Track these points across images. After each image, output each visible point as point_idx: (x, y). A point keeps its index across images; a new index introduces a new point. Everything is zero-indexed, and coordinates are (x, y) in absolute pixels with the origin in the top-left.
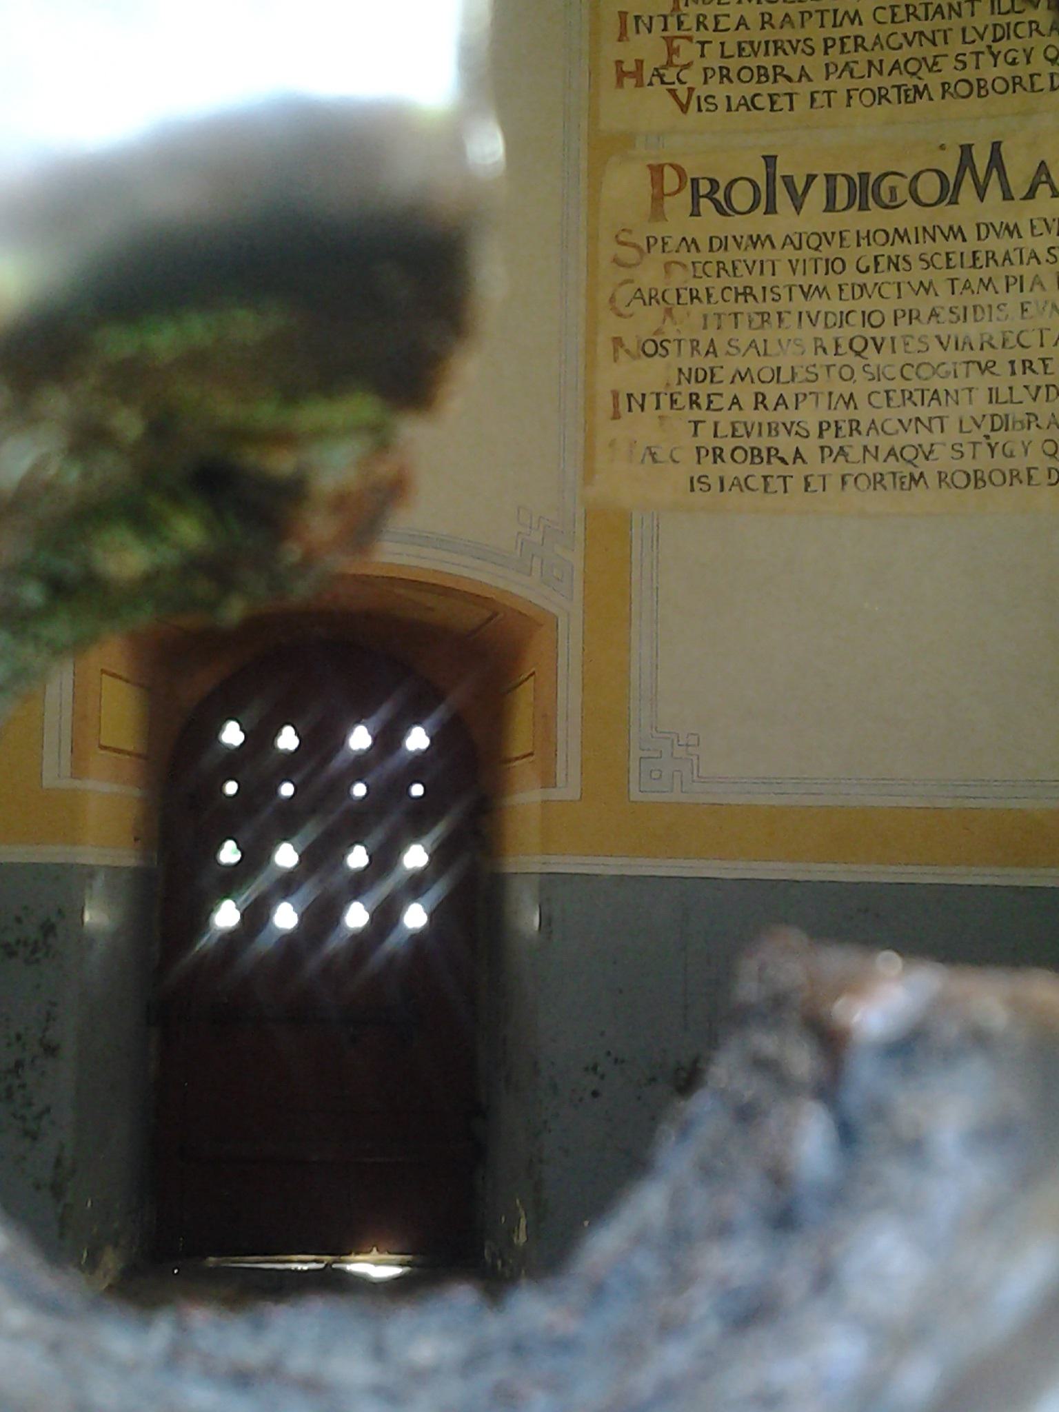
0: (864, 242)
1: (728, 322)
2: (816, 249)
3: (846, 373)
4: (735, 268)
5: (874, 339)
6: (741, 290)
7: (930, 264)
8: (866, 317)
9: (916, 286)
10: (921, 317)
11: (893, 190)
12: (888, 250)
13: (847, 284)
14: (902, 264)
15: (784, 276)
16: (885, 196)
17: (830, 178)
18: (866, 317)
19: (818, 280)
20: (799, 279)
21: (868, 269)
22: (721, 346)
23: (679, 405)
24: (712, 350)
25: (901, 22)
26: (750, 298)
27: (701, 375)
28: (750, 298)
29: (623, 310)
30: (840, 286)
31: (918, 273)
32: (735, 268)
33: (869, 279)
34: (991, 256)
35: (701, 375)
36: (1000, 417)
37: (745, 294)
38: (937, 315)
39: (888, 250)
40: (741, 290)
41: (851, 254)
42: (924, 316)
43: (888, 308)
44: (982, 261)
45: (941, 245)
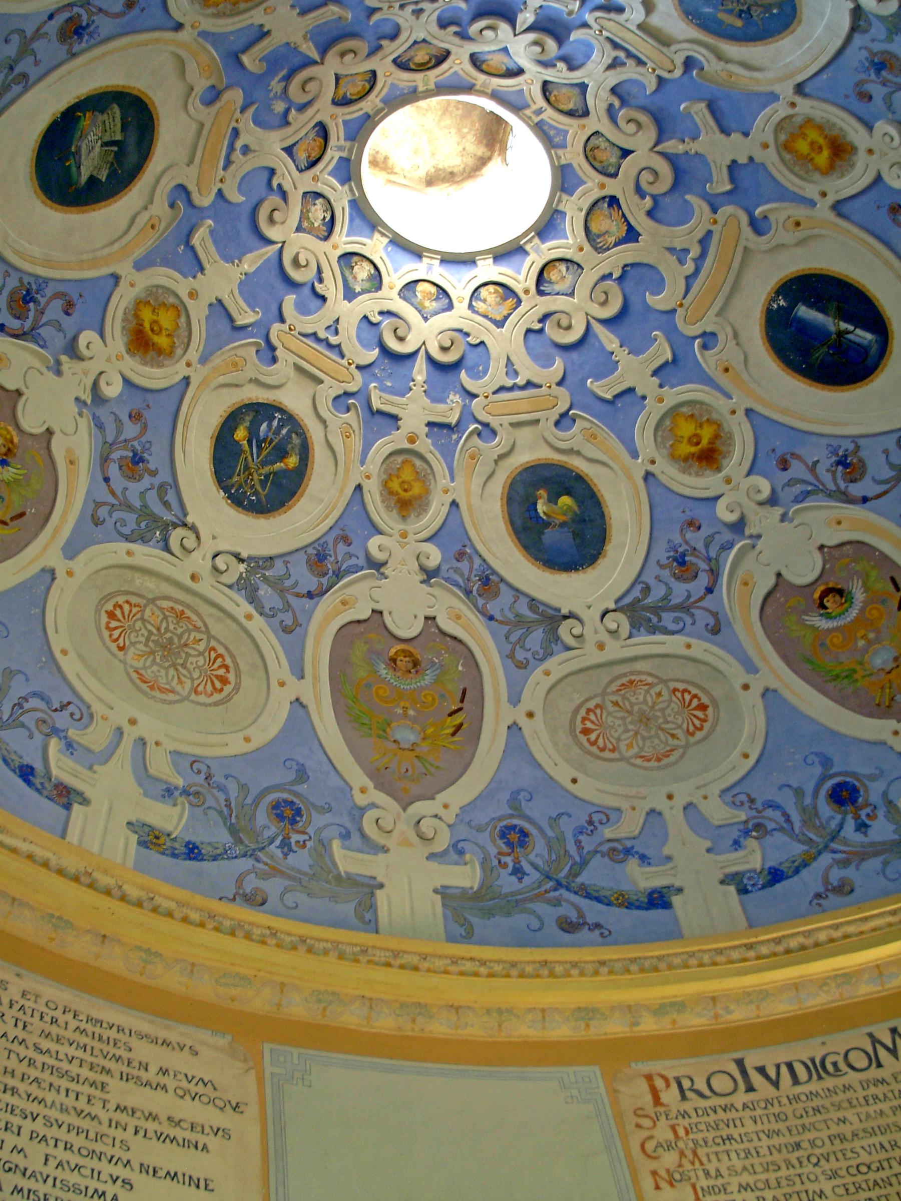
0: (793, 1102)
1: (724, 1157)
2: (766, 1108)
3: (812, 1177)
4: (717, 1125)
5: (822, 1155)
6: (725, 1137)
7: (839, 1108)
8: (812, 1143)
9: (836, 1120)
10: (73, 1148)
11: (835, 1064)
12: (811, 1104)
13: (55, 1158)
14: (822, 1110)
15: (750, 1127)
16: (830, 1068)
17: (790, 1066)
18: (812, 1143)
19: (775, 1126)
20: (759, 1127)
21: (802, 1116)
22: (724, 1172)
23: (15, 1113)
24: (719, 1174)
25: (160, 1178)
26: (733, 1141)
27: (717, 1190)
28: (733, 1141)
29: (653, 1155)
30: (47, 1155)
31: (835, 1115)
32: (717, 1125)
33: (806, 1121)
34: (876, 1098)
35: (717, 1190)
36: (676, 1181)
37: (729, 1139)
38: (857, 1135)
39: (811, 1104)
40: (725, 1137)
41: (788, 1110)
42: (849, 1136)
43: (824, 1134)
44: (871, 1101)
45: (842, 1096)
